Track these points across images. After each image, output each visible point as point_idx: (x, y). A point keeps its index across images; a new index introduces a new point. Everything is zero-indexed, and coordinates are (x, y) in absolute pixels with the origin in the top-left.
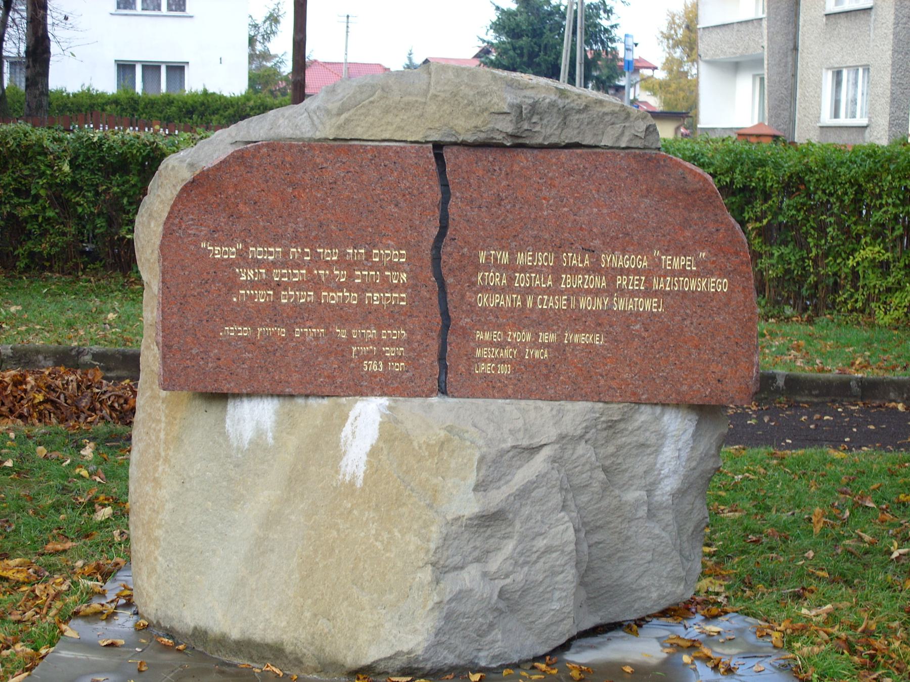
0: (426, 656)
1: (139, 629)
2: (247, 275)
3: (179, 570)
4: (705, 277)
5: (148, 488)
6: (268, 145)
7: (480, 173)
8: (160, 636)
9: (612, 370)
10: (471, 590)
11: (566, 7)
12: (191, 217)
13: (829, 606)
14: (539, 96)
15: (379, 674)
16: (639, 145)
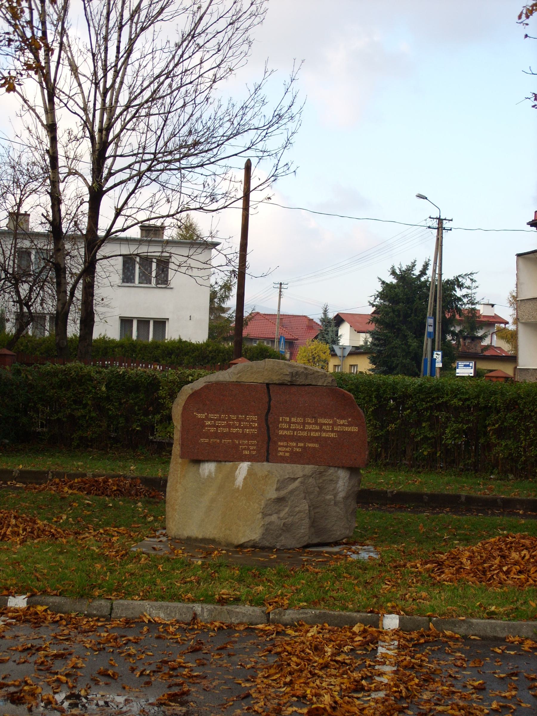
9: (323, 455)
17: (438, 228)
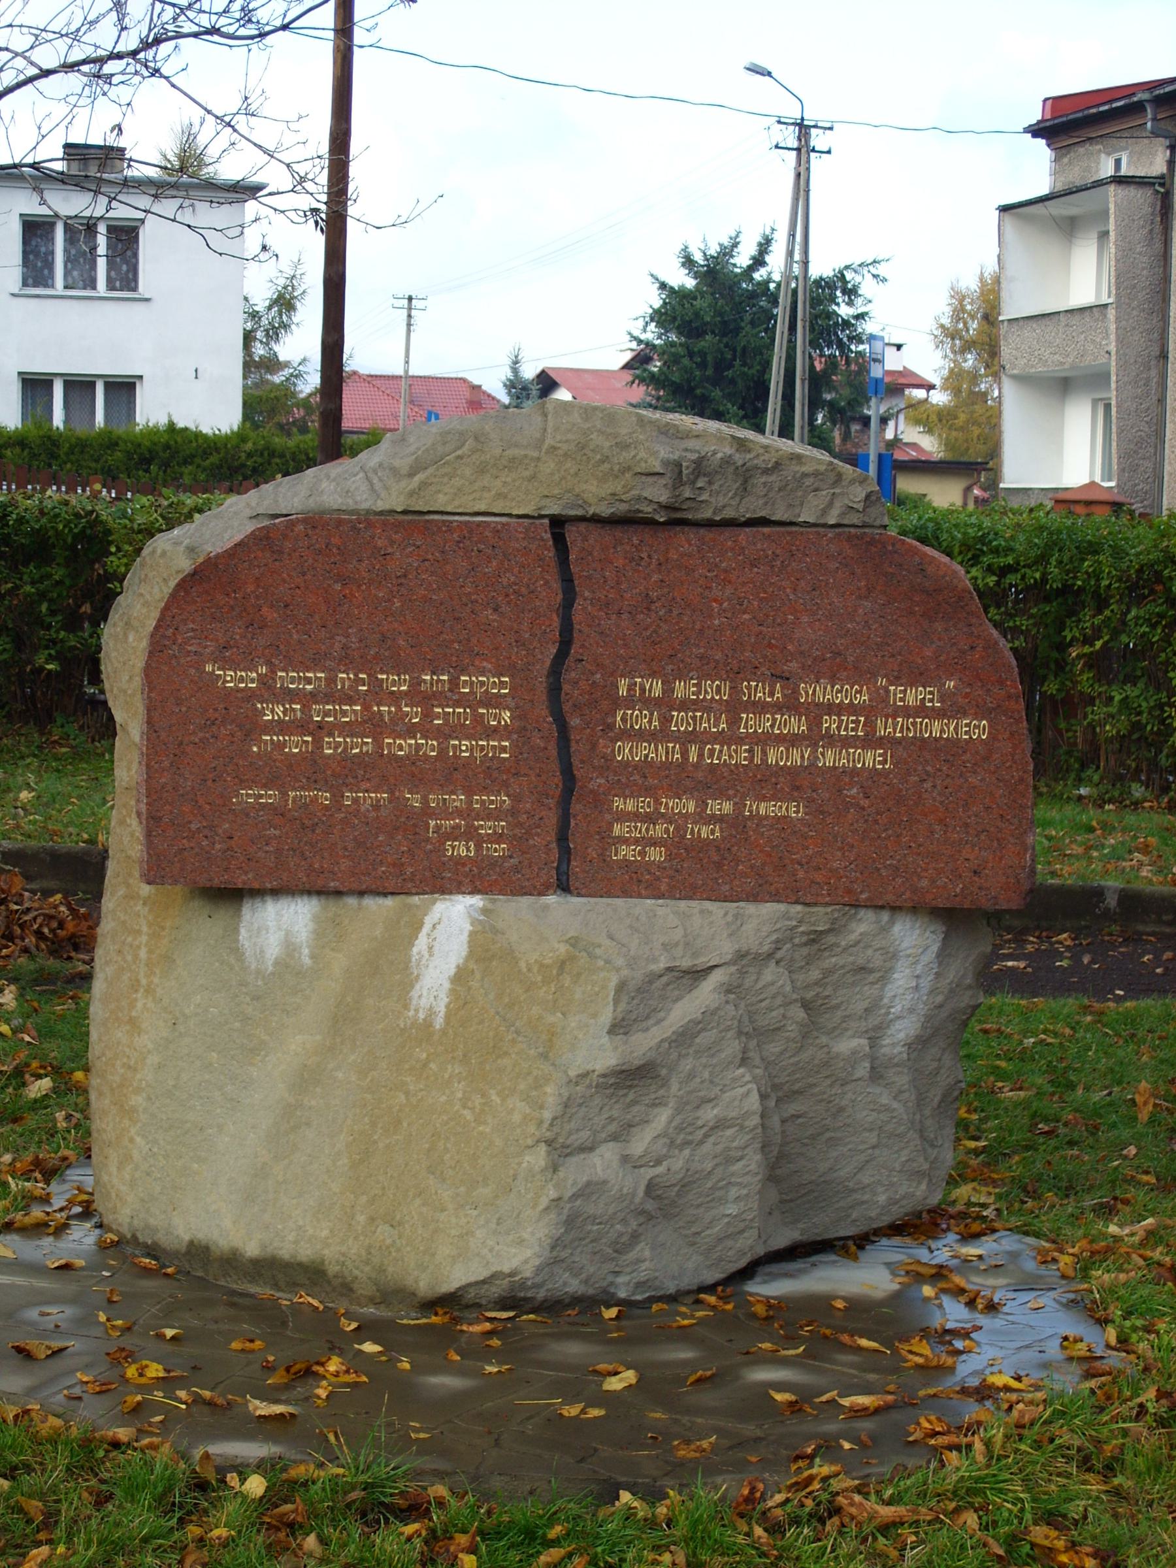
0: (538, 1280)
1: (103, 1247)
2: (274, 712)
3: (166, 1157)
4: (954, 717)
5: (120, 1034)
6: (305, 521)
7: (619, 562)
8: (137, 1256)
9: (817, 856)
10: (605, 1182)
11: (779, 285)
12: (191, 626)
13: (1150, 1220)
14: (706, 449)
15: (467, 1307)
16: (856, 521)
17: (798, 150)
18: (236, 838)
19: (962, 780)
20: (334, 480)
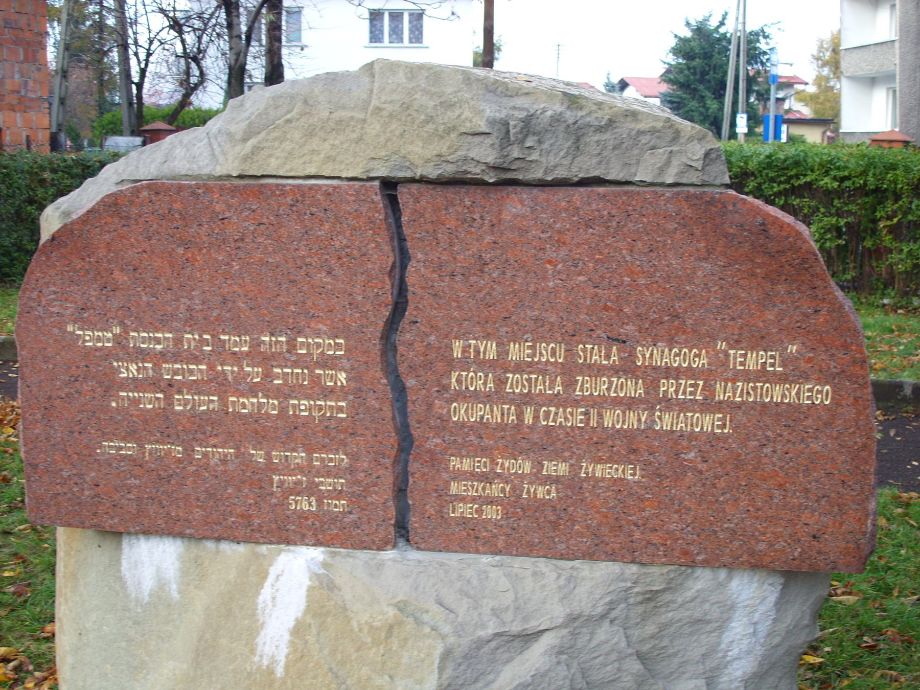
6: (149, 187)
7: (452, 224)
9: (660, 517)
12: (53, 289)
14: (535, 107)
16: (694, 180)
18: (101, 486)
19: (803, 446)
20: (185, 146)
